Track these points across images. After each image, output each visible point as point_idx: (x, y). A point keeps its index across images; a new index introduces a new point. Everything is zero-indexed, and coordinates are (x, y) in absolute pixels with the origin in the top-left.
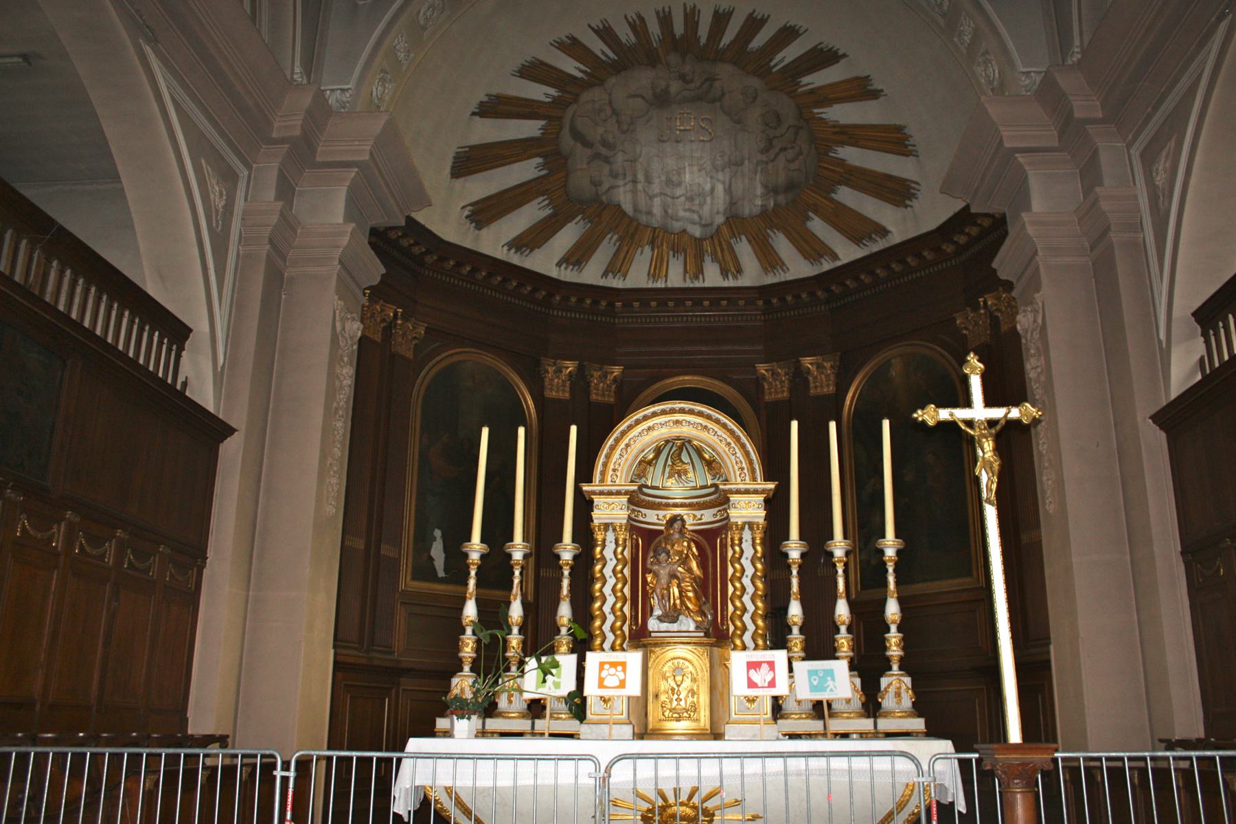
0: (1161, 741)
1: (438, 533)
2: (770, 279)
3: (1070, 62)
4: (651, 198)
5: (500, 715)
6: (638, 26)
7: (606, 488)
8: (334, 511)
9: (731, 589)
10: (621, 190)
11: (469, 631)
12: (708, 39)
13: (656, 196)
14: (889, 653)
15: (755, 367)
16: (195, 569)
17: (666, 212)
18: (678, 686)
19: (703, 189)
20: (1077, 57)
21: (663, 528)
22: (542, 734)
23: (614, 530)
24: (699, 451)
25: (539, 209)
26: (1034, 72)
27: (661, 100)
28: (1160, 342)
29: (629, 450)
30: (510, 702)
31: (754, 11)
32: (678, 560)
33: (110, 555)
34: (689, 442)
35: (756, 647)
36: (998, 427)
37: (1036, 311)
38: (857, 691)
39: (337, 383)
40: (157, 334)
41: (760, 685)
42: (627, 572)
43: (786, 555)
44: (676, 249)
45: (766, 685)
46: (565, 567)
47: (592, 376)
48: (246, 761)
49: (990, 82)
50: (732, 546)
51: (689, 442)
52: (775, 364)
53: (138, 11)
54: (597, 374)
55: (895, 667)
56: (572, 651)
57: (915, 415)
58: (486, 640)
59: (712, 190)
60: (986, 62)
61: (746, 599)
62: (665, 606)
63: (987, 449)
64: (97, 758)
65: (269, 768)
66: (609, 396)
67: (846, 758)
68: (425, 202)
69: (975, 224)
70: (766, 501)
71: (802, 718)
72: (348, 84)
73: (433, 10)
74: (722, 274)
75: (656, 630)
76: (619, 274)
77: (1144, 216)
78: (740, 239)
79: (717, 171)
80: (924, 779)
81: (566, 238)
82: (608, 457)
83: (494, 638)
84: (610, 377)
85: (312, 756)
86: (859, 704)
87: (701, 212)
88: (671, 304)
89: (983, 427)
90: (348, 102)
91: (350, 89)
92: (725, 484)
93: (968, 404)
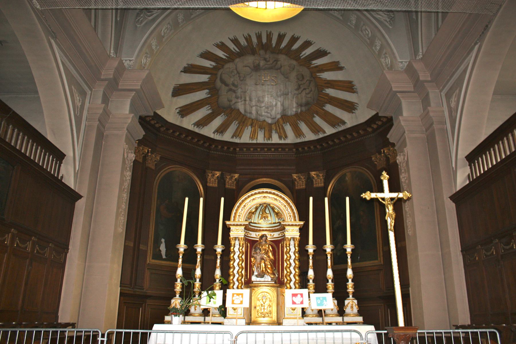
0: (454, 326)
1: (163, 240)
2: (299, 140)
3: (418, 58)
4: (252, 107)
5: (191, 315)
6: (248, 39)
7: (236, 223)
8: (122, 230)
9: (285, 264)
10: (240, 104)
11: (179, 280)
12: (276, 45)
13: (254, 106)
14: (348, 290)
15: (292, 176)
16: (64, 254)
17: (257, 113)
18: (264, 303)
19: (272, 104)
20: (421, 56)
21: (258, 239)
22: (208, 323)
23: (239, 240)
24: (273, 209)
25: (207, 110)
26: (404, 62)
27: (257, 68)
28: (453, 168)
29: (245, 208)
30: (195, 309)
31: (294, 34)
32: (264, 253)
33: (29, 247)
34: (269, 205)
35: (296, 288)
36: (395, 201)
37: (404, 155)
38: (336, 306)
39: (124, 178)
40: (51, 156)
41: (297, 303)
42: (244, 257)
43: (307, 251)
44: (261, 128)
45: (300, 303)
46: (218, 255)
47: (227, 178)
48: (86, 334)
49: (387, 65)
50: (286, 247)
51: (269, 205)
52: (300, 174)
53: (49, 26)
54: (228, 177)
55: (351, 296)
56: (221, 289)
57: (362, 196)
58: (186, 284)
59: (276, 105)
60: (386, 57)
61: (292, 268)
62: (259, 271)
63: (390, 210)
64: (22, 333)
65: (95, 337)
66: (233, 186)
67: (332, 333)
68: (163, 107)
69: (380, 120)
70: (300, 229)
71: (314, 317)
72: (132, 58)
73: (167, 30)
74: (279, 138)
75: (255, 281)
76: (238, 137)
77: (446, 118)
78: (287, 124)
79: (278, 97)
80: (363, 341)
81: (217, 122)
82: (237, 210)
83: (189, 283)
84: (234, 178)
85: (114, 332)
86: (336, 311)
87: (271, 113)
88: (259, 149)
89: (388, 201)
90: (132, 65)
91: (133, 60)
92: (284, 222)
93: (382, 190)
